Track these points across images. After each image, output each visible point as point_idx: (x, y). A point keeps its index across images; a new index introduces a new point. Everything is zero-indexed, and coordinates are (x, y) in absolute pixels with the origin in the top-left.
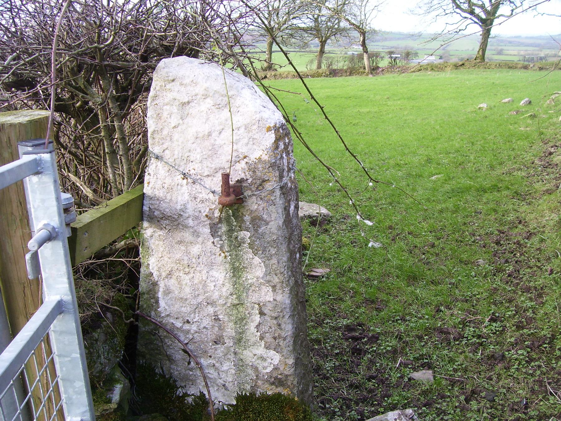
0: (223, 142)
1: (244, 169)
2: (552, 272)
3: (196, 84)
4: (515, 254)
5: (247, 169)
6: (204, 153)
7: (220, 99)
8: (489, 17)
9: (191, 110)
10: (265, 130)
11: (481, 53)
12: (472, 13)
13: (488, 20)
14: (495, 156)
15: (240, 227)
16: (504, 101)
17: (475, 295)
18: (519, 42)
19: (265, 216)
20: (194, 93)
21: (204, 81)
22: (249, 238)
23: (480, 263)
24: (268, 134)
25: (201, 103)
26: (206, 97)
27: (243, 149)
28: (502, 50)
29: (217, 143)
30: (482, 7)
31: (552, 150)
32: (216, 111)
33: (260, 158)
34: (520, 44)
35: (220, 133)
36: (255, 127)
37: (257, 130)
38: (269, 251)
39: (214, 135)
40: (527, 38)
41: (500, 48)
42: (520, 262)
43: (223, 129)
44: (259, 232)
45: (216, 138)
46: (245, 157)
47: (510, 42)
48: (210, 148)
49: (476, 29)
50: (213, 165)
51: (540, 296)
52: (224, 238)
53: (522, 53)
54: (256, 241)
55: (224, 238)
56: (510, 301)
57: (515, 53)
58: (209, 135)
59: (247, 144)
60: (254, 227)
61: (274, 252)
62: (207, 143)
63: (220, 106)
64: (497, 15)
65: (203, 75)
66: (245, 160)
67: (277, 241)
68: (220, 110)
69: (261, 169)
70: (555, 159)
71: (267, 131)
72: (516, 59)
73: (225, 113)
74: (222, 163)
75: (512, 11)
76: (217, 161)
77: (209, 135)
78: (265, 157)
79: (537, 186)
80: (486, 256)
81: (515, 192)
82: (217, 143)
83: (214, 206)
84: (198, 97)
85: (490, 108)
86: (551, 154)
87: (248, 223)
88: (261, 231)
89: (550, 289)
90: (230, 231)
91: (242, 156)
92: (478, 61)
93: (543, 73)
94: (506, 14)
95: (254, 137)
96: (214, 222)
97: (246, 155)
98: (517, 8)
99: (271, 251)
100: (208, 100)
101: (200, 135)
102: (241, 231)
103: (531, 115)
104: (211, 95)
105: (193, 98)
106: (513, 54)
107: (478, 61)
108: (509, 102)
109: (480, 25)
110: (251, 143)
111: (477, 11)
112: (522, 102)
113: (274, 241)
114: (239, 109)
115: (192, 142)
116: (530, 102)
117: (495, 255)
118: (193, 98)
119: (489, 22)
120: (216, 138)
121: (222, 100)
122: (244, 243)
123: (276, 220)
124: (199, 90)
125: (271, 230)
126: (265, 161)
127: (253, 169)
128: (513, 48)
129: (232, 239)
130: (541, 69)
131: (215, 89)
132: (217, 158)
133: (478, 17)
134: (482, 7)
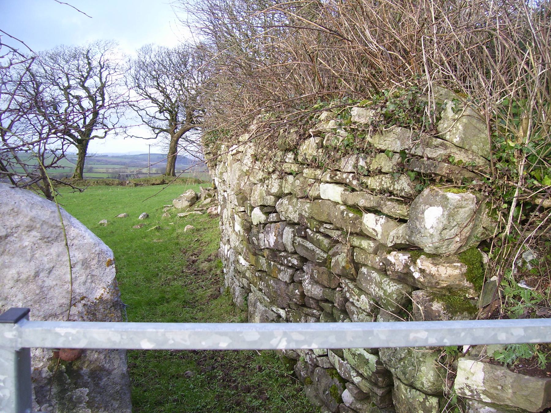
0: (54, 283)
1: (82, 313)
2: (260, 369)
3: (18, 213)
4: (216, 360)
5: (85, 313)
6: (29, 298)
7: (50, 230)
8: (84, 138)
9: (8, 245)
10: (104, 264)
11: (78, 171)
13: (84, 140)
14: (146, 269)
15: (75, 384)
16: (120, 216)
17: (204, 407)
18: (106, 161)
19: (107, 366)
20: (14, 224)
21: (29, 209)
22: (87, 395)
23: (189, 375)
24: (108, 269)
25: (24, 237)
26: (30, 228)
27: (79, 289)
28: (91, 168)
29: (46, 284)
31: (193, 258)
32: (44, 246)
33: (101, 298)
34: (107, 163)
35: (50, 272)
36: (94, 262)
37: (96, 266)
38: (112, 405)
39: (41, 275)
40: (113, 157)
41: (90, 166)
42: (224, 365)
43: (53, 267)
44: (101, 385)
45: (45, 279)
46: (83, 299)
47: (98, 161)
48: (38, 292)
49: (73, 150)
50: (41, 313)
51: (261, 392)
52: (54, 402)
53: (110, 171)
54: (97, 397)
55: (54, 402)
56: (238, 404)
57: (104, 170)
58: (37, 275)
59: (85, 283)
60: (94, 381)
61: (117, 406)
62: (32, 286)
63: (50, 239)
64: (91, 136)
65: (25, 201)
66: (83, 302)
67: (120, 392)
68: (49, 244)
69: (102, 310)
70: (201, 266)
71: (108, 265)
72: (105, 176)
73: (57, 248)
74: (53, 309)
75: (106, 132)
76: (47, 307)
77: (37, 275)
78: (107, 296)
79: (199, 292)
80: (192, 367)
81: (184, 301)
82: (46, 284)
83: (42, 364)
84: (20, 230)
85: (112, 223)
86: (194, 262)
87: (86, 377)
88: (103, 383)
89: (266, 384)
90: (63, 391)
91: (78, 298)
92: (76, 179)
93: (138, 188)
94: (100, 136)
95: (94, 273)
96: (41, 384)
97: (85, 295)
98: (110, 130)
99: (114, 405)
100: (34, 233)
101: (24, 277)
102: (77, 388)
103: (157, 228)
104: (38, 226)
105: (14, 230)
106: (102, 171)
107: (76, 179)
108: (125, 216)
109: (77, 146)
110: (90, 281)
112: (141, 216)
113: (117, 392)
114: (73, 242)
115: (10, 285)
116: (148, 216)
117: (198, 364)
118: (14, 230)
119: (84, 142)
120: (45, 279)
121: (52, 232)
122: (81, 403)
123: (119, 367)
125: (115, 380)
126: (107, 300)
129: (64, 401)
130: (136, 185)
131: (44, 220)
132: (46, 303)
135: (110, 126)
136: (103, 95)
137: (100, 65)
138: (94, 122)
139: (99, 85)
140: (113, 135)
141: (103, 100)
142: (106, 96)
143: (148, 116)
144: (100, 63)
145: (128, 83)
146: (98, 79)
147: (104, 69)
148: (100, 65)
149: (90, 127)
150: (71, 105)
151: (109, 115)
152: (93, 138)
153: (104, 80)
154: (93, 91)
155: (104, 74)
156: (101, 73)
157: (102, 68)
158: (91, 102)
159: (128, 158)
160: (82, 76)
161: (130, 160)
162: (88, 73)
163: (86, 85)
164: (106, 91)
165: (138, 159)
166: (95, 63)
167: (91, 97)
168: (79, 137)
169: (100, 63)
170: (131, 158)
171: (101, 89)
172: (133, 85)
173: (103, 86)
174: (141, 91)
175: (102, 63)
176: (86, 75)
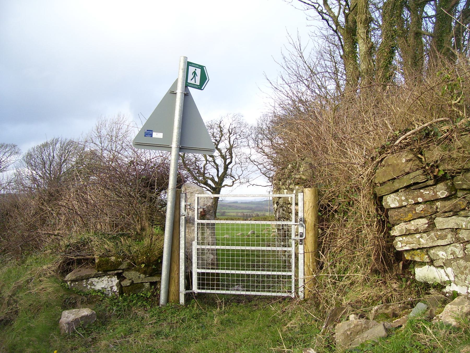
12: (206, 184)
18: (236, 206)
27: (205, 203)
28: (224, 212)
30: (213, 180)
34: (237, 208)
40: (242, 203)
41: (223, 211)
47: (230, 206)
53: (239, 214)
64: (223, 185)
75: (233, 182)
98: (236, 180)
111: (210, 182)
119: (217, 189)
124: (196, 189)
127: (208, 207)
128: (233, 211)
133: (210, 186)
134: (213, 180)
135: (237, 178)
136: (231, 154)
137: (229, 131)
138: (225, 175)
139: (228, 146)
140: (238, 184)
141: (232, 158)
142: (233, 155)
143: (265, 169)
144: (229, 130)
145: (250, 144)
146: (227, 142)
147: (232, 135)
148: (229, 131)
149: (222, 179)
150: (208, 162)
151: (235, 169)
152: (224, 186)
153: (232, 143)
154: (223, 151)
155: (232, 138)
156: (230, 138)
157: (230, 134)
158: (222, 160)
159: (254, 204)
160: (216, 140)
161: (255, 206)
162: (221, 138)
163: (219, 147)
164: (234, 151)
165: (262, 204)
166: (225, 131)
167: (224, 157)
168: (214, 186)
169: (229, 130)
170: (256, 204)
171: (230, 150)
172: (253, 145)
173: (231, 147)
174: (260, 150)
175: (230, 131)
176: (218, 139)
